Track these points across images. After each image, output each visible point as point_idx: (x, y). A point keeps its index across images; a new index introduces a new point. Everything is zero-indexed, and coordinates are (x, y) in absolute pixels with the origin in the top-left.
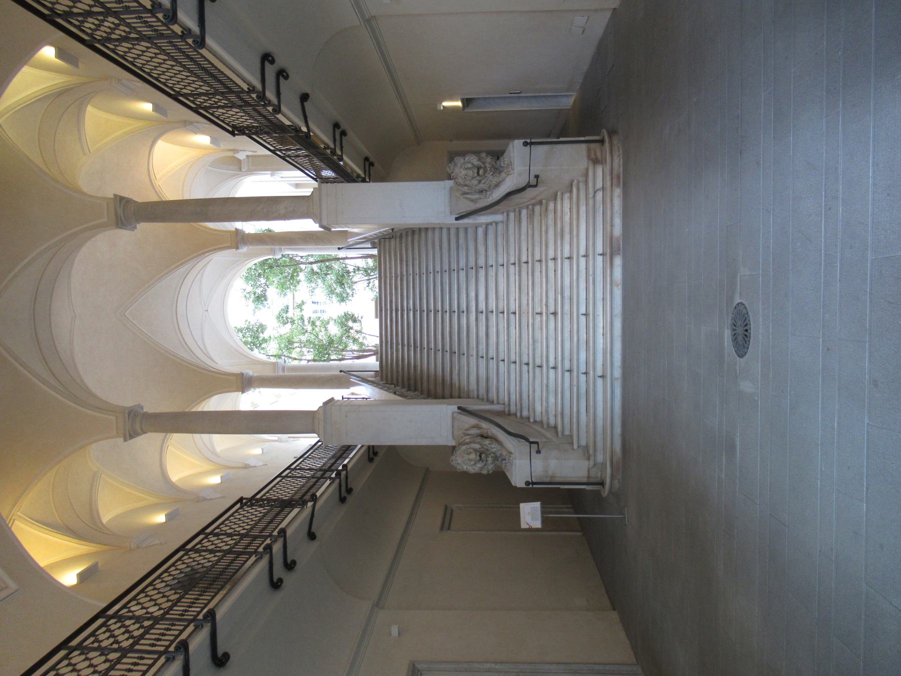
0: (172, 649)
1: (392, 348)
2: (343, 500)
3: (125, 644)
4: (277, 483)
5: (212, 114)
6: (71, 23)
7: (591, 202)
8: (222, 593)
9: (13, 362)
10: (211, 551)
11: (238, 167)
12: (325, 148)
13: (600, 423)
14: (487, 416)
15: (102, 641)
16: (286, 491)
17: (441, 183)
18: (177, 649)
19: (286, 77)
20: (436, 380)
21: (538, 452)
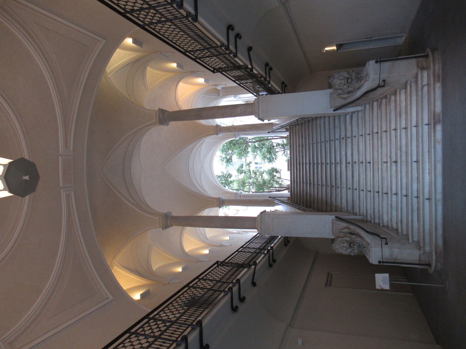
0: (179, 339)
2: (271, 266)
3: (157, 334)
4: (236, 255)
5: (203, 61)
6: (133, 16)
7: (420, 93)
9: (114, 190)
10: (202, 289)
11: (219, 94)
14: (354, 222)
16: (241, 259)
17: (325, 91)
18: (182, 340)
19: (240, 38)
21: (386, 244)
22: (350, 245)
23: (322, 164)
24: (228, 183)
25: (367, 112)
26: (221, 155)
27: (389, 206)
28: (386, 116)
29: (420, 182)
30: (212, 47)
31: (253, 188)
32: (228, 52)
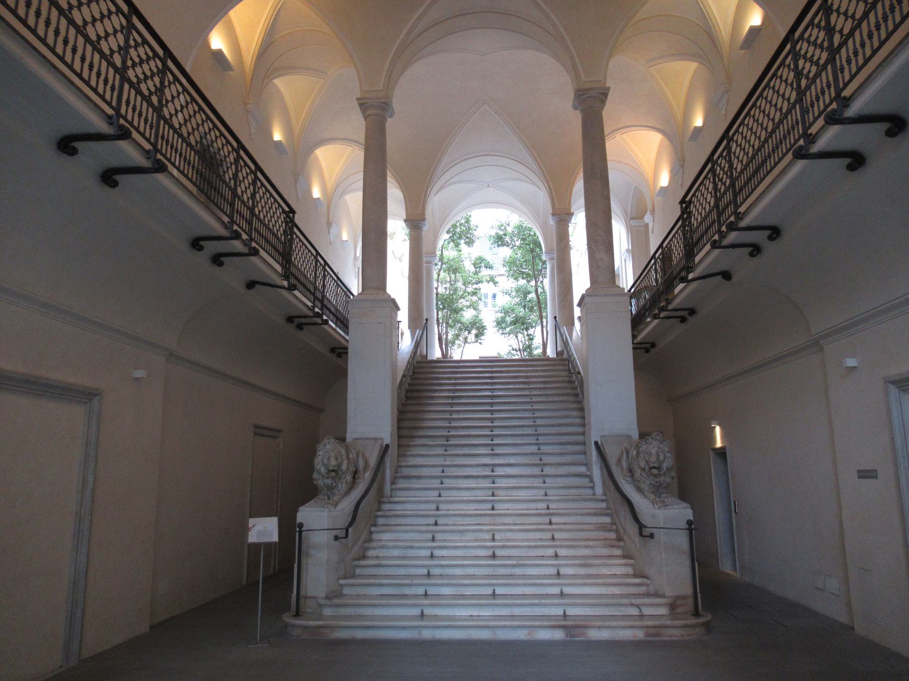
0: (122, 121)
1: (452, 373)
2: (290, 319)
3: (131, 74)
4: (309, 251)
5: (706, 177)
7: (626, 601)
8: (194, 190)
10: (235, 176)
11: (635, 218)
12: (667, 300)
13: (368, 611)
14: (378, 479)
15: (136, 50)
16: (300, 259)
17: (635, 426)
18: (121, 127)
19: (751, 255)
20: (418, 420)
21: (336, 538)
24: (455, 238)
25: (592, 505)
26: (512, 224)
29: (454, 599)
30: (735, 195)
31: (446, 288)
32: (724, 228)
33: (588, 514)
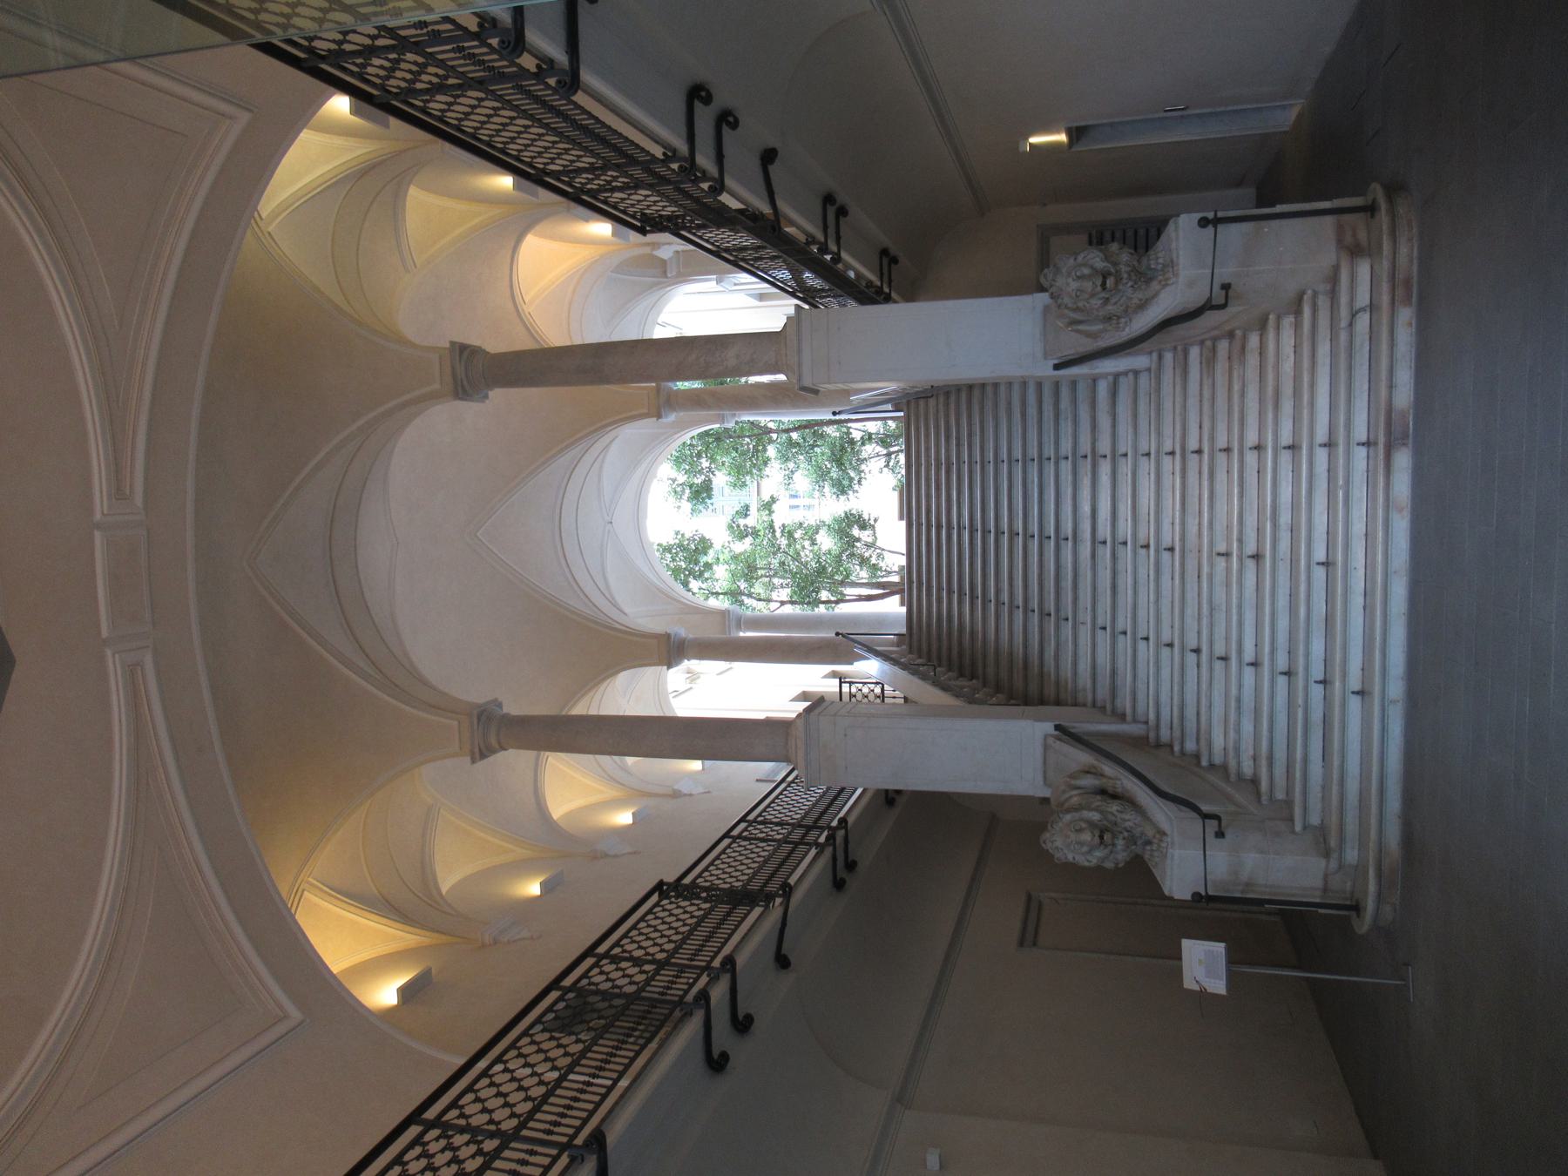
7: (1343, 336)
12: (808, 243)
13: (1353, 786)
16: (735, 873)
19: (734, 125)
21: (1220, 834)
22: (1101, 837)
23: (1013, 534)
25: (1168, 376)
26: (673, 473)
27: (1233, 704)
28: (1230, 399)
33: (1185, 388)
